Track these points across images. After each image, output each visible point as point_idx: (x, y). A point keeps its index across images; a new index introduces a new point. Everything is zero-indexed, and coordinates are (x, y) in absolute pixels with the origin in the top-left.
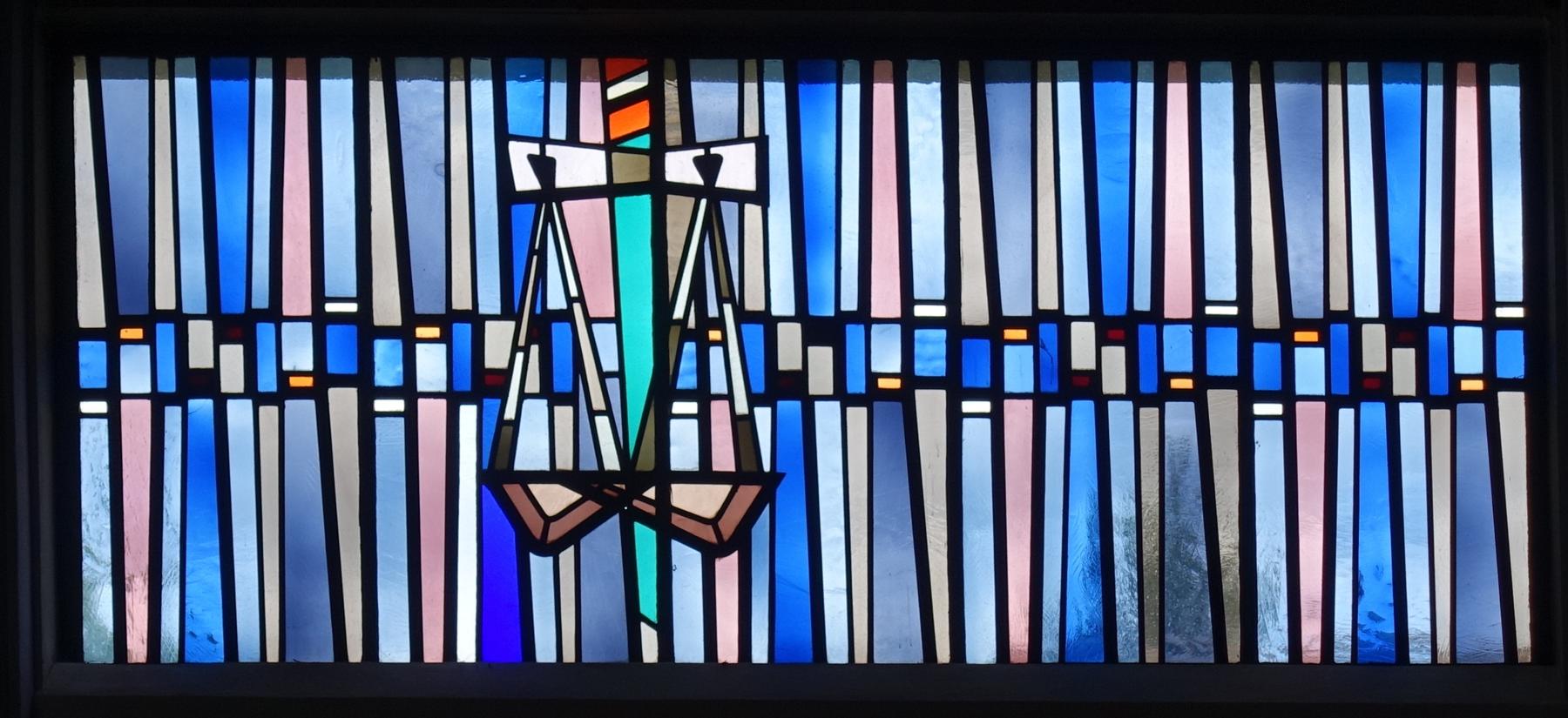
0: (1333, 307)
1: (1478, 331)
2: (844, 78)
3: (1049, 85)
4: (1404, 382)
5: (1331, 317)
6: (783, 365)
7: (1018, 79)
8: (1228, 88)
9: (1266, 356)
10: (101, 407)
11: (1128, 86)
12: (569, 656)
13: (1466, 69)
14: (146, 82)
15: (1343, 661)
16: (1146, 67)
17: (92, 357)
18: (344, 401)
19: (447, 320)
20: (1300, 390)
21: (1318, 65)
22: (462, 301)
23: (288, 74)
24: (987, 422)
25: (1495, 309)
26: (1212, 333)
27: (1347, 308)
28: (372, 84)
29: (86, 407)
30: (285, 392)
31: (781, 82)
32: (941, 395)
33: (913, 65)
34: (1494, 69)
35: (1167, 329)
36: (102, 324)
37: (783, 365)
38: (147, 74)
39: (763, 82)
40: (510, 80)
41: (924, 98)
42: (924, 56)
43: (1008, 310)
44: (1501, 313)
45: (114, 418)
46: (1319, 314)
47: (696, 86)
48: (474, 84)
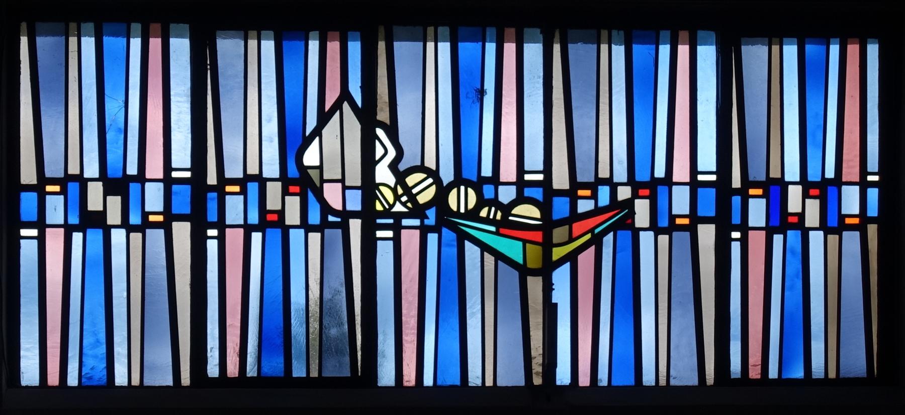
2: (680, 39)
3: (778, 47)
5: (600, 181)
8: (514, 45)
10: (34, 232)
11: (595, 46)
13: (510, 32)
14: (125, 40)
21: (124, 26)
22: (604, 173)
25: (171, 172)
27: (258, 173)
29: (24, 232)
30: (145, 225)
31: (25, 36)
33: (528, 32)
34: (173, 26)
35: (674, 188)
36: (35, 182)
37: (270, 206)
39: (247, 39)
40: (809, 44)
41: (533, 52)
48: (440, 44)
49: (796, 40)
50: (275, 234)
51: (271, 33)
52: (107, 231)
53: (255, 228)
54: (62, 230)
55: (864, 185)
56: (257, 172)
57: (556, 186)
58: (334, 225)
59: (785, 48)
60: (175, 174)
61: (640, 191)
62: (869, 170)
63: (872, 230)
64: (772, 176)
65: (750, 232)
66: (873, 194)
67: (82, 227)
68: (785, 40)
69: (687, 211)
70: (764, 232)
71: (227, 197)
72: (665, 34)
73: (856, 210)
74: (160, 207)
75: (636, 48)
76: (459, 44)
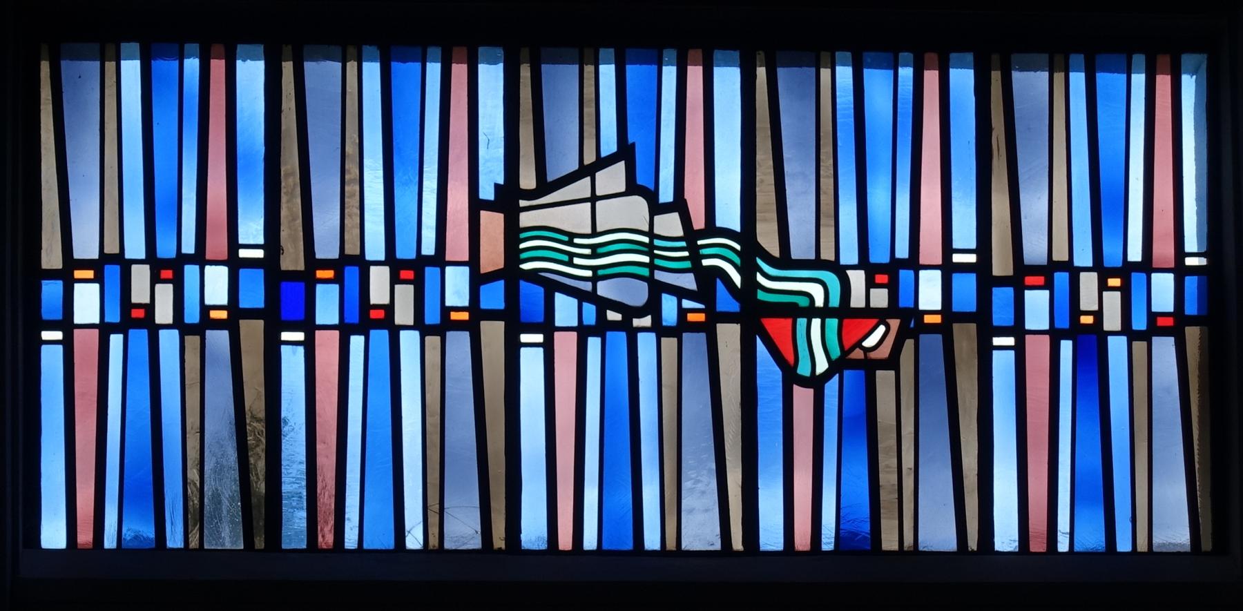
1: (938, 273)
3: (114, 63)
4: (404, 314)
6: (169, 288)
8: (465, 67)
9: (1002, 297)
11: (1124, 76)
13: (1164, 60)
16: (434, 51)
17: (51, 291)
19: (98, 266)
20: (1028, 326)
29: (46, 335)
30: (445, 325)
32: (973, 327)
37: (169, 288)
39: (1131, 74)
41: (728, 80)
43: (78, 254)
44: (957, 258)
46: (1119, 264)
47: (866, 71)
49: (260, 49)
50: (140, 337)
51: (135, 47)
52: (394, 332)
53: (115, 328)
54: (337, 333)
55: (235, 265)
56: (1066, 258)
58: (615, 326)
61: (163, 271)
63: (1193, 334)
64: (107, 251)
67: (123, 327)
68: (240, 48)
69: (78, 287)
70: (575, 334)
72: (670, 54)
75: (630, 70)
76: (925, 71)
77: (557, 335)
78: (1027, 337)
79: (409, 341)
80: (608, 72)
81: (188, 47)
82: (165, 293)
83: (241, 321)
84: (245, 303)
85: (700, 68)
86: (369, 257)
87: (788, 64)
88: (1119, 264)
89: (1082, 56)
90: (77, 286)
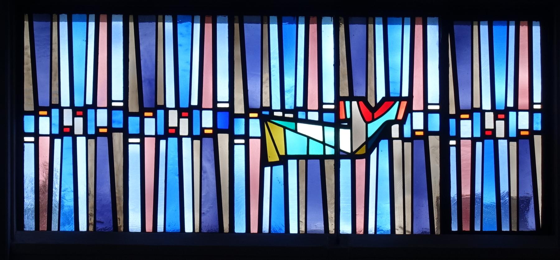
0: (53, 103)
1: (527, 113)
2: (270, 22)
5: (263, 108)
6: (81, 119)
7: (150, 21)
10: (32, 139)
12: (197, 230)
13: (103, 17)
14: (506, 27)
15: (197, 232)
16: (407, 20)
18: (118, 138)
23: (218, 21)
24: (139, 146)
26: (430, 116)
27: (58, 103)
28: (25, 22)
29: (26, 139)
33: (219, 18)
34: (429, 19)
36: (243, 112)
37: (81, 119)
38: (133, 20)
42: (433, 16)
44: (219, 105)
45: (36, 143)
47: (246, 25)
54: (49, 138)
55: (532, 111)
57: (130, 110)
59: (352, 27)
60: (114, 104)
62: (535, 101)
65: (461, 140)
66: (538, 118)
71: (250, 120)
72: (197, 18)
73: (421, 127)
74: (211, 125)
76: (416, 25)
77: (40, 138)
78: (40, 137)
79: (81, 142)
80: (274, 28)
81: (272, 18)
82: (501, 124)
83: (535, 136)
84: (430, 129)
85: (211, 25)
86: (273, 108)
87: (39, 20)
88: (503, 108)
89: (94, 15)
90: (41, 118)
